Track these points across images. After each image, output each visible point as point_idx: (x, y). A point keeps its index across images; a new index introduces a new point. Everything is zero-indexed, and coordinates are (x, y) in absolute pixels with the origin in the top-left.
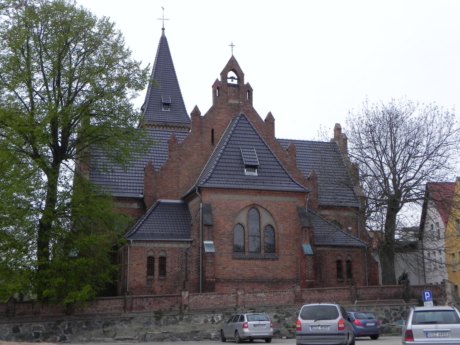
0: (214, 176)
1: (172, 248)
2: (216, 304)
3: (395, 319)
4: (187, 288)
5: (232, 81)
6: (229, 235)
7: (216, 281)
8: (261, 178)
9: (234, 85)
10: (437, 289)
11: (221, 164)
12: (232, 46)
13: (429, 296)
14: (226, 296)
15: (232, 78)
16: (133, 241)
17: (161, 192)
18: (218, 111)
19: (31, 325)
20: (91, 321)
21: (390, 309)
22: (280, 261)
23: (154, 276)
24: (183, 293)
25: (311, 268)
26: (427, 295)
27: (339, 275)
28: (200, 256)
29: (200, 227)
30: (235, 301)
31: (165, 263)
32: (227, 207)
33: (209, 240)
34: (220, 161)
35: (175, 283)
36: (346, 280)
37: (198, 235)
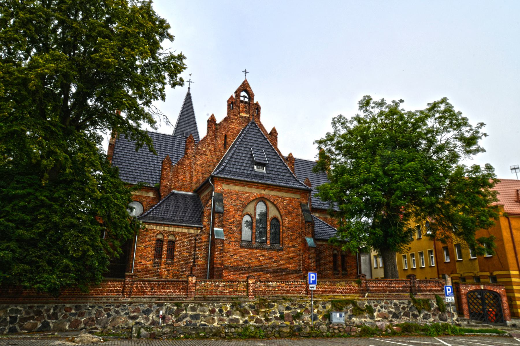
0: (226, 169)
1: (182, 233)
2: (224, 293)
3: (404, 314)
4: (194, 273)
5: (244, 99)
6: (238, 224)
7: (224, 268)
8: (269, 175)
9: (245, 102)
10: (439, 284)
11: (231, 163)
12: (246, 72)
13: (450, 292)
14: (236, 284)
15: (244, 97)
16: (143, 222)
17: (176, 183)
18: (232, 120)
19: (8, 307)
20: (82, 305)
21: (399, 303)
22: (284, 252)
23: (161, 260)
24: (190, 279)
25: (314, 260)
26: (449, 290)
27: (335, 268)
28: (209, 242)
29: (211, 214)
30: (245, 289)
31: (174, 247)
32: (238, 198)
33: (219, 227)
34: (233, 157)
35: (182, 268)
36: (341, 273)
37: (209, 223)
